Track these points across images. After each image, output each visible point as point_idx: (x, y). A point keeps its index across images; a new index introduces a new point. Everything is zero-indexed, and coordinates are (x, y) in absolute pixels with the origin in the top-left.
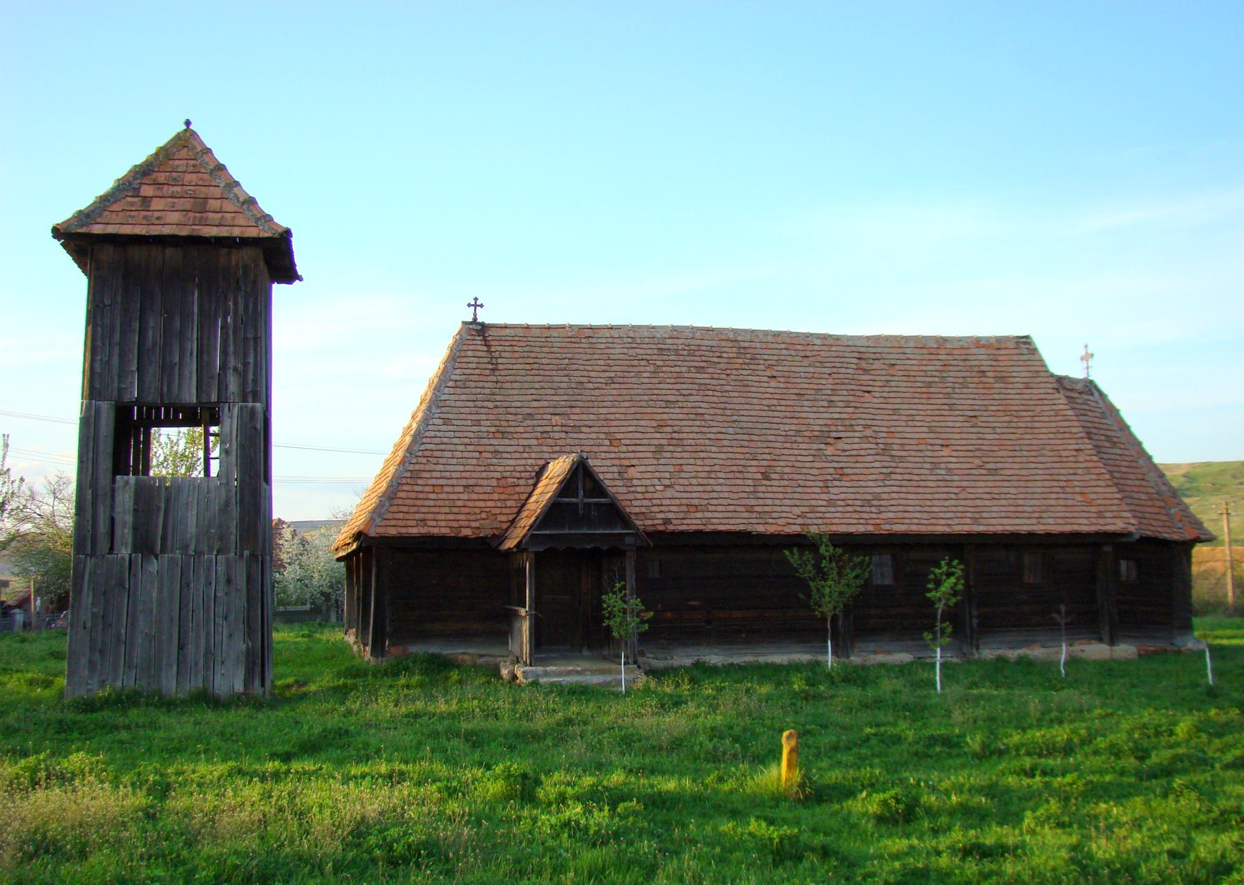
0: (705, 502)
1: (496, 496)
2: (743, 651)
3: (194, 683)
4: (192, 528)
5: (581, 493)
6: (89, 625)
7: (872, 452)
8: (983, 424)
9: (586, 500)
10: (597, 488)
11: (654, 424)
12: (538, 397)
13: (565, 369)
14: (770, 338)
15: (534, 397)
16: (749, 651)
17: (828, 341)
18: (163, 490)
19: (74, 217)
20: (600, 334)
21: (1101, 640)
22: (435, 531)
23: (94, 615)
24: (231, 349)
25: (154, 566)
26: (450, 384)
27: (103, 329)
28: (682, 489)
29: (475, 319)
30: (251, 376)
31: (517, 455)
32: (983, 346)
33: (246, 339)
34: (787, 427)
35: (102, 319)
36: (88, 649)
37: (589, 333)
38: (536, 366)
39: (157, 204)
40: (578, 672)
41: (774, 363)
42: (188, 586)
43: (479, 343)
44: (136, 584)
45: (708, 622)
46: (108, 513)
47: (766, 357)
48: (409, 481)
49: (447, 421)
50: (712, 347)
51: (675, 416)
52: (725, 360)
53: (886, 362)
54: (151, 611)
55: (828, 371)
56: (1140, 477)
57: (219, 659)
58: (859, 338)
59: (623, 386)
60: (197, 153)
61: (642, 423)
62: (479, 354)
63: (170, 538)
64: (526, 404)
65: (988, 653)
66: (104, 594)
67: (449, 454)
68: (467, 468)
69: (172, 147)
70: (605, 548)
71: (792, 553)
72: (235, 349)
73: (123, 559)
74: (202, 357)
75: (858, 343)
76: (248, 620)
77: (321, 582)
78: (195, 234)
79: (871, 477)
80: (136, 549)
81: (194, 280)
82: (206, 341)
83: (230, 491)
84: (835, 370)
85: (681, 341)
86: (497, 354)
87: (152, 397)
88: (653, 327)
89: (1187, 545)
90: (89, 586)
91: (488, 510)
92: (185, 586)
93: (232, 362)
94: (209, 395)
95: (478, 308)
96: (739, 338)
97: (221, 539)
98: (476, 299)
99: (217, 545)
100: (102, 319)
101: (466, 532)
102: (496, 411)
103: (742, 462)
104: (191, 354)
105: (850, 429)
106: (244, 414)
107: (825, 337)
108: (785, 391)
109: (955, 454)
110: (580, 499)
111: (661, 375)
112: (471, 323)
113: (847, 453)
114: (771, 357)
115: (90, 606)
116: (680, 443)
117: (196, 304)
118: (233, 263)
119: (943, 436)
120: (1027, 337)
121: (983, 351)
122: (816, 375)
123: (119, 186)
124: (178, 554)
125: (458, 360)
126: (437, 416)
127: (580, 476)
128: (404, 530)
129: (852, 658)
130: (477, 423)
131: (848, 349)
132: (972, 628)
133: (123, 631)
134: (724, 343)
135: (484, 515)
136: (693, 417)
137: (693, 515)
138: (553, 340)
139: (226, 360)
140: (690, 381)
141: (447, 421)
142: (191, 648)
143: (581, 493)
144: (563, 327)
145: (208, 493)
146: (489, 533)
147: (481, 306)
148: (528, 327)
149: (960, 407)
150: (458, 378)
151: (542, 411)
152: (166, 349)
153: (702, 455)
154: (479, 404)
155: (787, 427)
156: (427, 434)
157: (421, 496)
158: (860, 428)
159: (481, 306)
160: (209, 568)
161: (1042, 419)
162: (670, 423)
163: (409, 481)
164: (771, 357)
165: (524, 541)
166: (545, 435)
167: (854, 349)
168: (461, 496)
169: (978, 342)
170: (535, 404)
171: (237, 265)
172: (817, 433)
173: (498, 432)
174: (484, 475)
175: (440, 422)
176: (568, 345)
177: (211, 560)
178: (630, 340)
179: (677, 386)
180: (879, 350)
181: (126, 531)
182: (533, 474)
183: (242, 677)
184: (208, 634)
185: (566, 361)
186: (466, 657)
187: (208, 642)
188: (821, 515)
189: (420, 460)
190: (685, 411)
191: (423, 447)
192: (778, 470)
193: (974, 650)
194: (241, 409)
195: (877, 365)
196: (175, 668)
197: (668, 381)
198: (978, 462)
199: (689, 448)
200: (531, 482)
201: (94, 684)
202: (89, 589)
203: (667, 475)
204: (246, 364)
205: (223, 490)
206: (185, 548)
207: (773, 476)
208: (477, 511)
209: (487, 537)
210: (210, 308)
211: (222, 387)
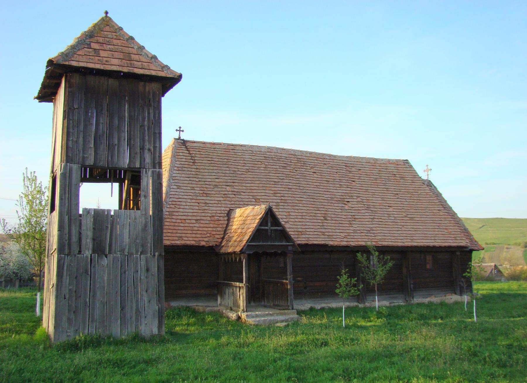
1: (212, 225)
3: (131, 330)
4: (126, 240)
5: (269, 224)
6: (67, 297)
7: (363, 208)
8: (401, 198)
10: (276, 221)
11: (272, 192)
12: (218, 177)
13: (226, 164)
14: (308, 155)
15: (216, 177)
16: (322, 302)
19: (59, 55)
20: (237, 148)
21: (456, 294)
23: (70, 290)
24: (147, 138)
25: (105, 261)
26: (176, 168)
27: (73, 122)
28: (292, 223)
29: (180, 137)
31: (215, 205)
32: (392, 163)
33: (155, 133)
34: (327, 196)
35: (73, 116)
36: (67, 311)
37: (232, 147)
38: (212, 162)
40: (271, 315)
41: (313, 166)
42: (125, 273)
43: (184, 149)
45: (305, 288)
46: (78, 229)
47: (309, 163)
48: (169, 217)
49: (179, 187)
50: (286, 157)
51: (280, 189)
53: (357, 168)
56: (457, 222)
57: (143, 315)
58: (343, 157)
63: (113, 245)
66: (76, 278)
67: (184, 204)
68: (195, 211)
70: (280, 252)
71: (362, 255)
72: (149, 138)
73: (87, 257)
77: (14, 267)
78: (131, 71)
79: (366, 220)
80: (94, 251)
81: (125, 98)
82: (132, 133)
83: (147, 218)
84: (338, 171)
86: (193, 155)
87: (103, 163)
88: (259, 147)
89: (471, 251)
90: (67, 273)
92: (123, 273)
93: (147, 146)
94: (135, 163)
95: (181, 132)
96: (296, 154)
97: (143, 246)
98: (180, 128)
99: (140, 250)
100: (73, 116)
101: (203, 243)
102: (200, 183)
103: (314, 212)
104: (124, 140)
106: (155, 175)
107: (330, 156)
109: (394, 210)
110: (269, 227)
111: (268, 169)
114: (311, 164)
115: (68, 285)
116: (285, 201)
117: (126, 112)
118: (147, 90)
119: (388, 202)
120: (407, 160)
121: (392, 165)
122: (331, 173)
123: (79, 41)
124: (119, 255)
125: (176, 157)
126: (173, 184)
127: (269, 216)
128: (173, 242)
129: (366, 304)
132: (411, 288)
133: (88, 300)
134: (291, 156)
135: (208, 235)
136: (287, 189)
138: (217, 150)
139: (144, 144)
141: (179, 187)
143: (269, 224)
144: (220, 144)
145: (135, 219)
146: (214, 244)
147: (183, 131)
148: (204, 143)
149: (390, 190)
150: (179, 166)
151: (221, 184)
152: (110, 136)
153: (297, 208)
154: (192, 179)
155: (327, 196)
156: (171, 193)
157: (176, 224)
159: (183, 131)
160: (137, 263)
161: (421, 196)
162: (279, 192)
163: (169, 217)
164: (311, 164)
166: (225, 196)
167: (343, 162)
168: (195, 225)
169: (389, 161)
170: (217, 180)
171: (149, 92)
172: (339, 199)
174: (203, 214)
175: (175, 187)
176: (225, 153)
177: (137, 258)
178: (251, 152)
179: (277, 175)
180: (353, 163)
181: (88, 240)
183: (157, 325)
184: (137, 301)
186: (200, 308)
187: (137, 305)
188: (352, 237)
189: (171, 206)
190: (284, 186)
191: (171, 200)
192: (329, 215)
193: (412, 299)
194: (153, 172)
195: (353, 169)
196: (119, 321)
197: (272, 172)
198: (404, 214)
199: (290, 204)
200: (226, 218)
202: (67, 276)
203: (284, 217)
205: (143, 218)
206: (122, 251)
207: (328, 218)
208: (205, 232)
209: (213, 246)
211: (142, 159)
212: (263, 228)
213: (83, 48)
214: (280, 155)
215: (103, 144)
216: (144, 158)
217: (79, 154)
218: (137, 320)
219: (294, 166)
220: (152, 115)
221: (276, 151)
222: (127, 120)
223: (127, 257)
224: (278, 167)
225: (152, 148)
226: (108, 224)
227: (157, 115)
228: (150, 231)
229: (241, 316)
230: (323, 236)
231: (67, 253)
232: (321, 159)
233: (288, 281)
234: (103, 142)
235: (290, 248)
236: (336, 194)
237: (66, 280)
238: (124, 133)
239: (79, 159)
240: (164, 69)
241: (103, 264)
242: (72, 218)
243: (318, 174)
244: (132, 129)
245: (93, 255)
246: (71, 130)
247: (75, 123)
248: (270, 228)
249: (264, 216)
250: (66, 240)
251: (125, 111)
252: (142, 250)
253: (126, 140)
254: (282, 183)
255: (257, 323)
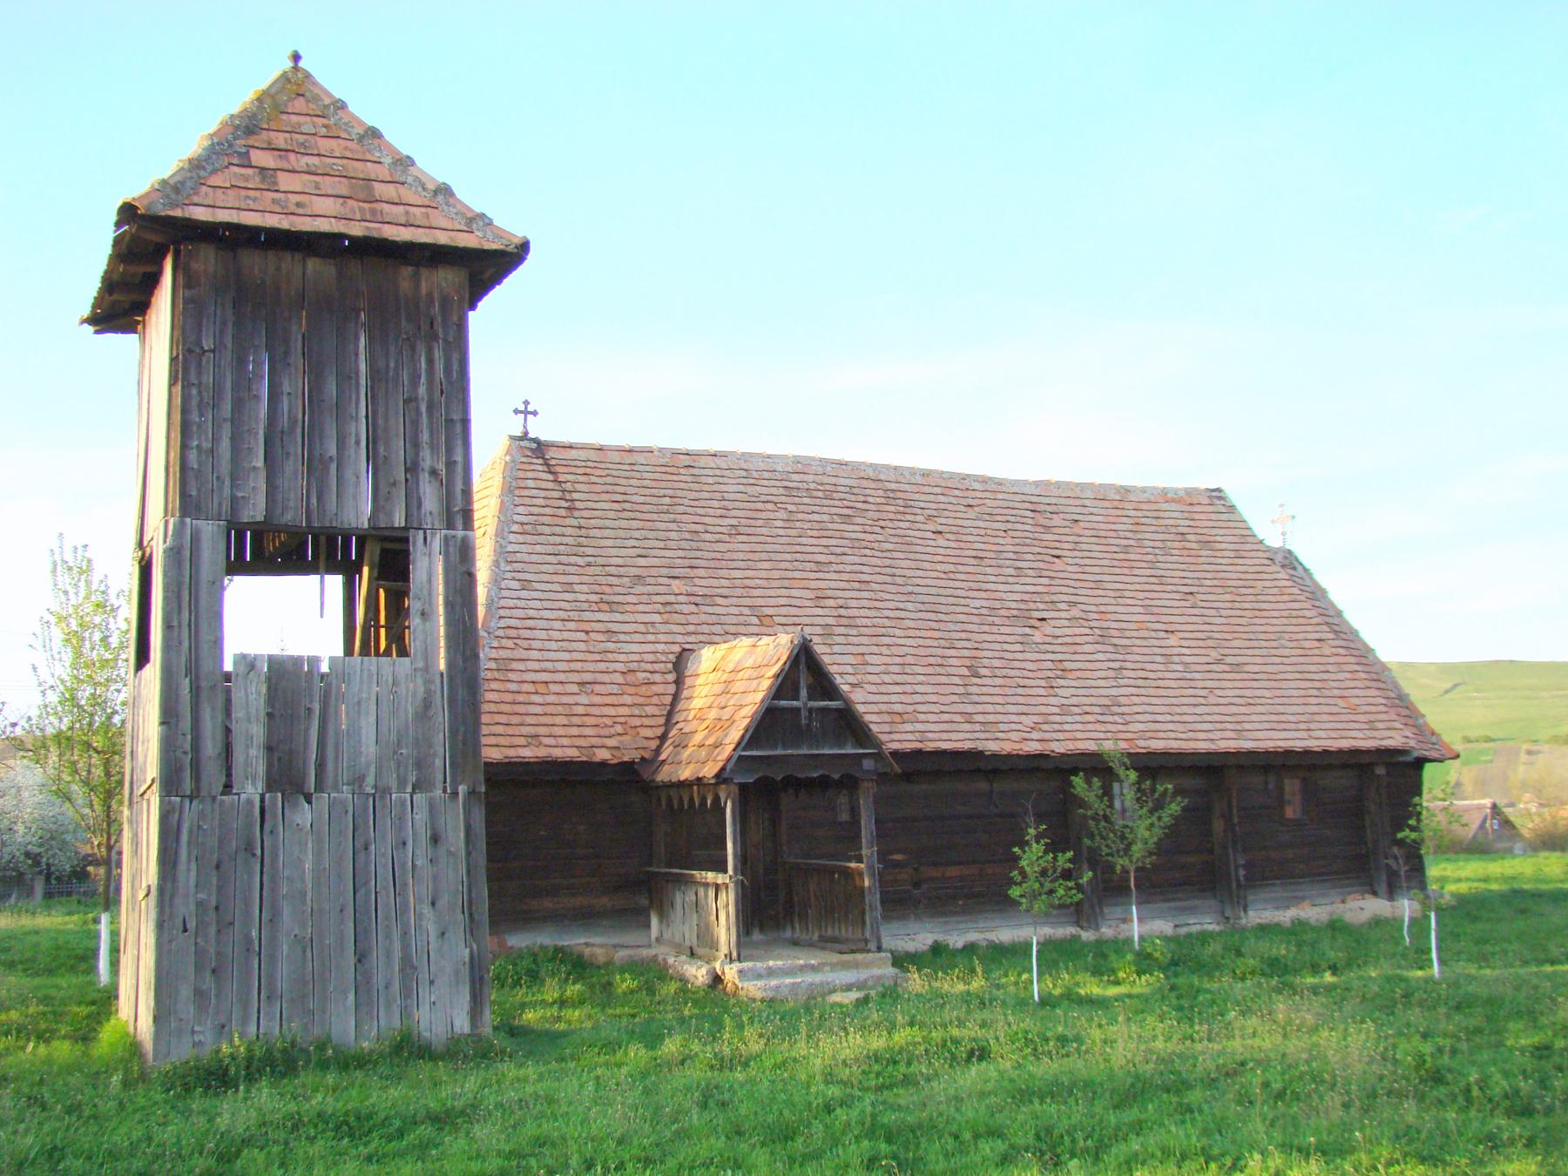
0: (910, 709)
1: (628, 699)
2: (962, 926)
3: (387, 1022)
4: (369, 748)
5: (804, 693)
8: (1203, 604)
9: (812, 704)
10: (823, 684)
11: (811, 595)
12: (644, 552)
14: (919, 479)
15: (639, 551)
16: (970, 925)
17: (992, 486)
18: (317, 679)
19: (154, 190)
22: (558, 753)
24: (425, 436)
25: (304, 815)
26: (515, 528)
27: (200, 393)
28: (873, 688)
29: (526, 433)
30: (459, 486)
31: (638, 637)
32: (1173, 501)
33: (450, 422)
34: (977, 603)
35: (199, 373)
37: (686, 460)
38: (627, 506)
39: (285, 181)
40: (813, 968)
41: (934, 513)
42: (366, 849)
43: (541, 468)
44: (275, 847)
45: (917, 885)
48: (496, 674)
49: (526, 585)
50: (851, 487)
52: (873, 507)
54: (303, 894)
55: (1003, 526)
56: (1375, 677)
57: (424, 976)
59: (753, 539)
60: (327, 107)
61: (795, 593)
62: (544, 485)
63: (330, 766)
64: (629, 561)
65: (1259, 914)
66: (218, 867)
68: (576, 656)
69: (281, 91)
70: (836, 776)
71: (1088, 782)
74: (375, 449)
75: (1026, 490)
76: (470, 908)
77: (29, 838)
78: (375, 234)
79: (1099, 674)
80: (271, 785)
81: (358, 316)
82: (380, 421)
84: (1010, 526)
85: (810, 478)
86: (568, 486)
87: (292, 515)
89: (1420, 762)
90: (189, 853)
91: (622, 720)
92: (361, 848)
93: (427, 459)
94: (390, 515)
96: (882, 477)
97: (419, 765)
98: (526, 403)
99: (412, 778)
100: (199, 373)
101: (602, 755)
102: (591, 570)
103: (939, 652)
104: (358, 443)
105: (1051, 606)
107: (984, 480)
108: (958, 552)
109: (1184, 643)
110: (802, 701)
111: (798, 524)
112: (521, 439)
113: (1060, 641)
114: (929, 505)
115: (193, 890)
116: (851, 622)
117: (362, 357)
121: (1174, 507)
122: (989, 532)
124: (346, 793)
126: (509, 575)
127: (802, 667)
128: (511, 753)
129: (1103, 930)
130: (569, 587)
131: (1018, 498)
132: (1238, 880)
133: (255, 933)
134: (865, 483)
135: (619, 729)
136: (856, 585)
137: (901, 727)
139: (417, 454)
140: (838, 534)
141: (526, 585)
142: (376, 958)
143: (804, 693)
147: (535, 413)
151: (654, 572)
152: (313, 434)
155: (977, 603)
156: (503, 603)
157: (521, 698)
158: (1063, 606)
159: (535, 413)
160: (401, 818)
163: (496, 674)
165: (729, 767)
166: (668, 608)
169: (1165, 495)
170: (642, 562)
171: (430, 296)
172: (1015, 613)
173: (602, 601)
174: (602, 666)
175: (515, 585)
177: (403, 803)
178: (744, 473)
180: (1053, 501)
181: (253, 752)
182: (670, 666)
183: (466, 1007)
184: (405, 933)
185: (667, 500)
186: (598, 951)
187: (405, 947)
189: (505, 642)
190: (845, 576)
191: (503, 623)
193: (1242, 914)
194: (446, 539)
195: (1057, 520)
196: (351, 997)
197: (810, 533)
198: (1214, 654)
201: (206, 1035)
202: (189, 861)
203: (849, 669)
204: (450, 464)
205: (420, 681)
206: (358, 781)
207: (983, 671)
209: (633, 763)
210: (388, 366)
211: (413, 502)
212: (783, 703)
213: (227, 167)
214: (834, 480)
215: (292, 458)
216: (419, 499)
217: (221, 489)
218: (406, 992)
219: (876, 515)
220: (439, 366)
221: (820, 470)
222: (363, 382)
223: (371, 799)
224: (826, 518)
225: (441, 467)
226: (311, 702)
227: (455, 367)
228: (441, 719)
229: (723, 973)
230: (967, 727)
231: (188, 793)
232: (957, 492)
233: (862, 866)
234: (292, 450)
235: (868, 764)
236: (1004, 596)
237: (187, 873)
238: (357, 421)
239: (220, 504)
240: (475, 226)
241: (300, 822)
242: (204, 684)
243: (948, 536)
244: (381, 410)
245: (267, 795)
246: (195, 417)
247: (205, 394)
248: (805, 704)
249: (787, 667)
250: (185, 753)
251: (357, 355)
252: (418, 780)
253: (363, 443)
254: (841, 567)
255: (771, 994)
